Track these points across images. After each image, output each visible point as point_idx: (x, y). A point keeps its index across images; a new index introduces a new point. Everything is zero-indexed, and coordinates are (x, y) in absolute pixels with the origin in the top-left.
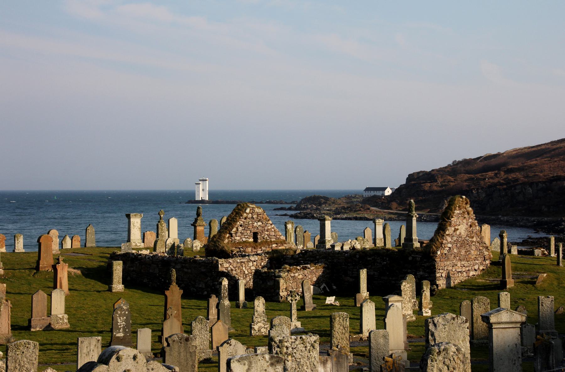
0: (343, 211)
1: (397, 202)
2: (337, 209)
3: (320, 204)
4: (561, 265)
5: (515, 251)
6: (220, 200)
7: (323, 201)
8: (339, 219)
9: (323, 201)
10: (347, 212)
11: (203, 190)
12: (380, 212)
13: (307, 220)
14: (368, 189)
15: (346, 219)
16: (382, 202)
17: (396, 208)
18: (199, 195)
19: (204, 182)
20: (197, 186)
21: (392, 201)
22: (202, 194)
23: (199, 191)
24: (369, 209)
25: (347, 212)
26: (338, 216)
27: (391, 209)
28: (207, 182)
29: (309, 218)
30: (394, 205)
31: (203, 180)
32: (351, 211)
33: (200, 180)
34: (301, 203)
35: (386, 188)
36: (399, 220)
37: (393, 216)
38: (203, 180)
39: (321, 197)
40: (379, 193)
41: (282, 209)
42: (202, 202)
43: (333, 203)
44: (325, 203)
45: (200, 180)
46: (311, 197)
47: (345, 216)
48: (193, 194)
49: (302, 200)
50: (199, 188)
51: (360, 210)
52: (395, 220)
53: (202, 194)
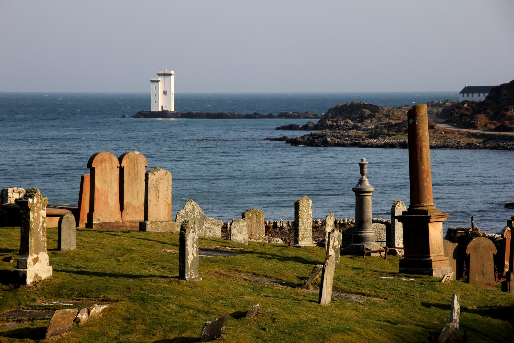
0: (385, 131)
1: (487, 115)
2: (377, 127)
3: (362, 119)
4: (191, 275)
5: (240, 232)
6: (227, 112)
7: (367, 112)
8: (372, 146)
9: (367, 112)
10: (391, 132)
11: (165, 93)
12: (452, 132)
14: (467, 90)
15: (378, 146)
16: (462, 115)
17: (485, 126)
18: (157, 102)
19: (167, 78)
20: (153, 85)
21: (479, 112)
22: (164, 101)
23: (157, 95)
25: (391, 132)
26: (373, 141)
27: (475, 128)
28: (172, 78)
30: (482, 119)
33: (159, 75)
34: (326, 116)
36: (485, 148)
37: (474, 141)
41: (291, 127)
42: (164, 114)
44: (371, 116)
45: (159, 75)
46: (345, 105)
47: (387, 140)
48: (147, 100)
49: (330, 110)
50: (157, 88)
52: (479, 148)
53: (164, 101)
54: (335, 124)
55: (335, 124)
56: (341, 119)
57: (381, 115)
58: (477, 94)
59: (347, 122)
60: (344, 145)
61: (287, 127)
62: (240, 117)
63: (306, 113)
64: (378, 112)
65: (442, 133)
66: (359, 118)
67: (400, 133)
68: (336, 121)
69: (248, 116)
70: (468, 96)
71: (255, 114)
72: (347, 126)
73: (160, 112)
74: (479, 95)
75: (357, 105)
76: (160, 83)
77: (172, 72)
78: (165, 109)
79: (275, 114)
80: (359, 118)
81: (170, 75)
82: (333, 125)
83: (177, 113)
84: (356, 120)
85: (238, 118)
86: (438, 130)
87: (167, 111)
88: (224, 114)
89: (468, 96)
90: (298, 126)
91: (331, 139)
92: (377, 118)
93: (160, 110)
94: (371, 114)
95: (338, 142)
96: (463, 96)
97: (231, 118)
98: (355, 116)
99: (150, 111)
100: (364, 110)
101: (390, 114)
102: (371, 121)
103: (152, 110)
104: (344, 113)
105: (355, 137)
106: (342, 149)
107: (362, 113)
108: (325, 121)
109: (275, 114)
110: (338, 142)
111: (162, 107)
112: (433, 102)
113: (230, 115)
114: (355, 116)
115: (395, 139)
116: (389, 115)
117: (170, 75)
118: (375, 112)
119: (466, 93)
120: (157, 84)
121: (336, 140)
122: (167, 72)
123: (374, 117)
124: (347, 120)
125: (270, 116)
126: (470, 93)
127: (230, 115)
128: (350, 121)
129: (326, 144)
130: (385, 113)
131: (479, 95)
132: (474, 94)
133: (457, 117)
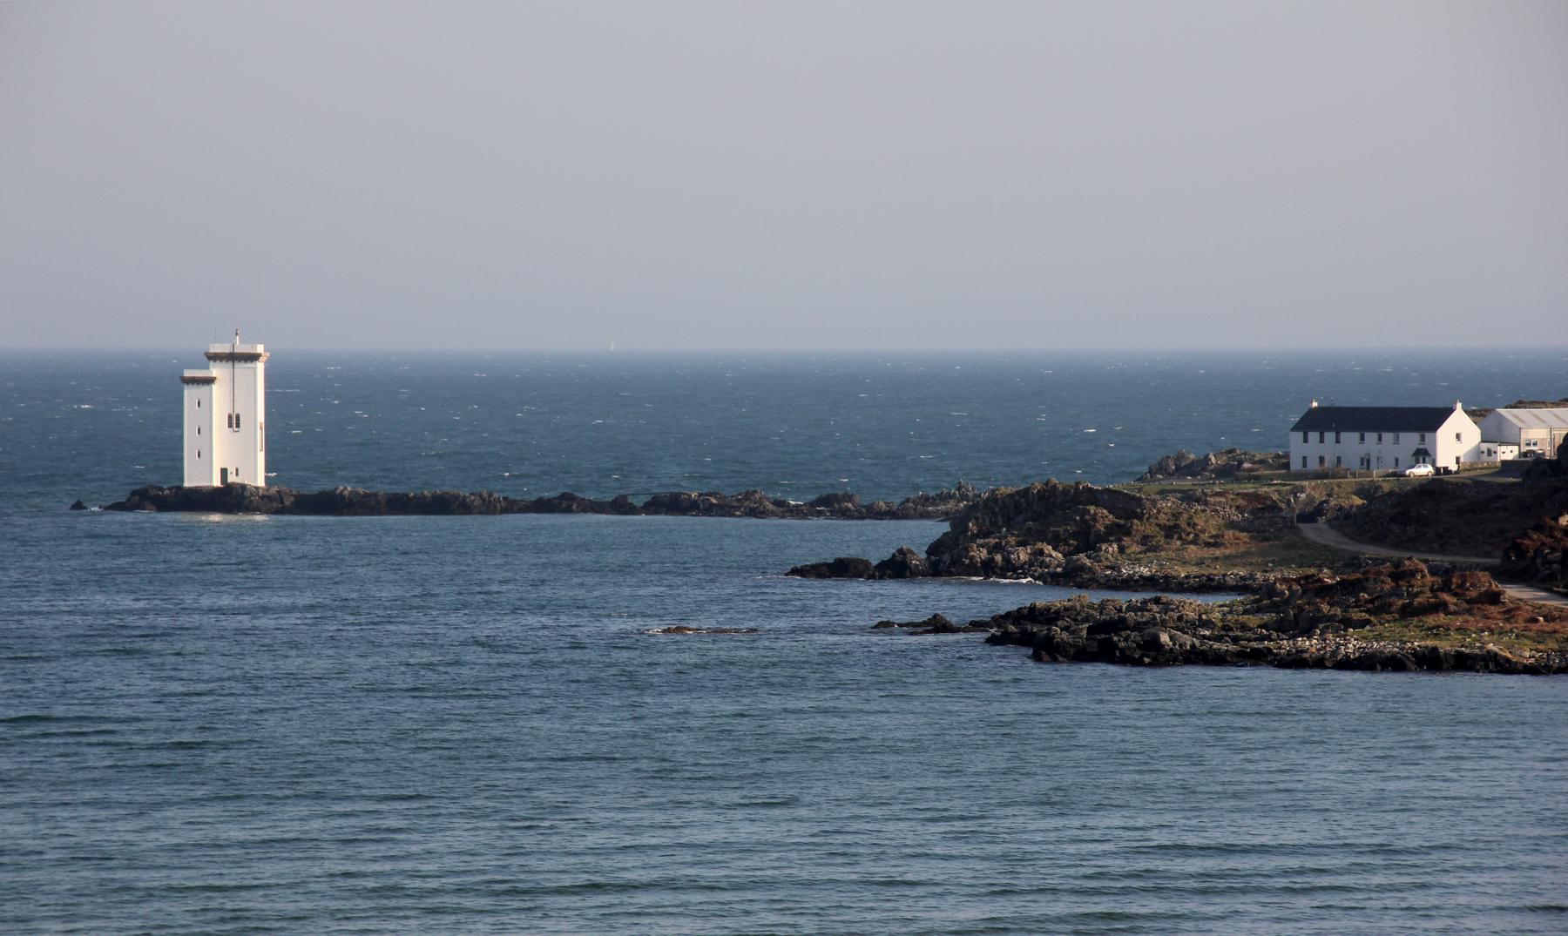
3: (1088, 540)
7: (1103, 517)
8: (1319, 663)
9: (1103, 517)
11: (234, 421)
13: (518, 516)
15: (1366, 663)
24: (1494, 598)
26: (1310, 645)
28: (260, 366)
29: (1125, 660)
31: (233, 358)
32: (1379, 607)
35: (1443, 414)
38: (233, 358)
39: (1093, 497)
40: (1386, 455)
42: (229, 498)
43: (1170, 531)
44: (1117, 532)
47: (1353, 645)
51: (1440, 607)
54: (998, 558)
55: (998, 558)
56: (1012, 540)
57: (1150, 529)
58: (1356, 436)
59: (1041, 552)
60: (1218, 660)
61: (828, 565)
62: (511, 507)
63: (748, 495)
64: (1140, 518)
65: (1537, 621)
66: (1074, 535)
67: (1387, 617)
68: (997, 548)
69: (542, 506)
70: (1322, 441)
71: (563, 497)
72: (1042, 564)
73: (217, 489)
74: (1362, 438)
75: (1065, 492)
76: (215, 387)
77: (260, 349)
78: (231, 479)
79: (639, 502)
80: (1074, 535)
81: (254, 357)
82: (992, 560)
83: (281, 496)
84: (1066, 543)
85: (505, 511)
86: (1519, 608)
87: (243, 487)
88: (456, 497)
89: (1322, 441)
90: (867, 563)
91: (1171, 638)
92: (1138, 538)
93: (217, 482)
94: (1118, 525)
95: (1193, 646)
96: (1306, 441)
97: (481, 513)
98: (1061, 530)
99: (180, 488)
100: (1092, 509)
101: (1182, 523)
102: (1122, 550)
103: (187, 484)
104: (1020, 518)
105: (1223, 628)
106: (1211, 671)
107: (1086, 522)
108: (966, 549)
109: (639, 502)
110: (1193, 646)
111: (224, 472)
112: (1180, 457)
113: (477, 502)
114: (1061, 530)
115: (1379, 638)
116: (1177, 526)
117: (254, 357)
118: (1128, 518)
119: (1314, 429)
120: (204, 389)
121: (1188, 640)
122: (241, 348)
123: (1128, 534)
124: (1039, 545)
125: (620, 506)
126: (1330, 429)
127: (477, 502)
128: (1048, 549)
129: (1152, 655)
130: (1163, 519)
131: (1362, 438)
132: (1343, 435)
133: (1551, 563)
